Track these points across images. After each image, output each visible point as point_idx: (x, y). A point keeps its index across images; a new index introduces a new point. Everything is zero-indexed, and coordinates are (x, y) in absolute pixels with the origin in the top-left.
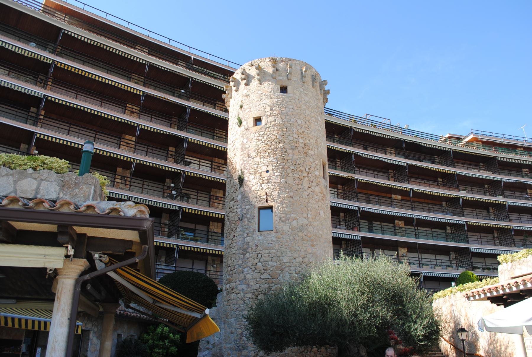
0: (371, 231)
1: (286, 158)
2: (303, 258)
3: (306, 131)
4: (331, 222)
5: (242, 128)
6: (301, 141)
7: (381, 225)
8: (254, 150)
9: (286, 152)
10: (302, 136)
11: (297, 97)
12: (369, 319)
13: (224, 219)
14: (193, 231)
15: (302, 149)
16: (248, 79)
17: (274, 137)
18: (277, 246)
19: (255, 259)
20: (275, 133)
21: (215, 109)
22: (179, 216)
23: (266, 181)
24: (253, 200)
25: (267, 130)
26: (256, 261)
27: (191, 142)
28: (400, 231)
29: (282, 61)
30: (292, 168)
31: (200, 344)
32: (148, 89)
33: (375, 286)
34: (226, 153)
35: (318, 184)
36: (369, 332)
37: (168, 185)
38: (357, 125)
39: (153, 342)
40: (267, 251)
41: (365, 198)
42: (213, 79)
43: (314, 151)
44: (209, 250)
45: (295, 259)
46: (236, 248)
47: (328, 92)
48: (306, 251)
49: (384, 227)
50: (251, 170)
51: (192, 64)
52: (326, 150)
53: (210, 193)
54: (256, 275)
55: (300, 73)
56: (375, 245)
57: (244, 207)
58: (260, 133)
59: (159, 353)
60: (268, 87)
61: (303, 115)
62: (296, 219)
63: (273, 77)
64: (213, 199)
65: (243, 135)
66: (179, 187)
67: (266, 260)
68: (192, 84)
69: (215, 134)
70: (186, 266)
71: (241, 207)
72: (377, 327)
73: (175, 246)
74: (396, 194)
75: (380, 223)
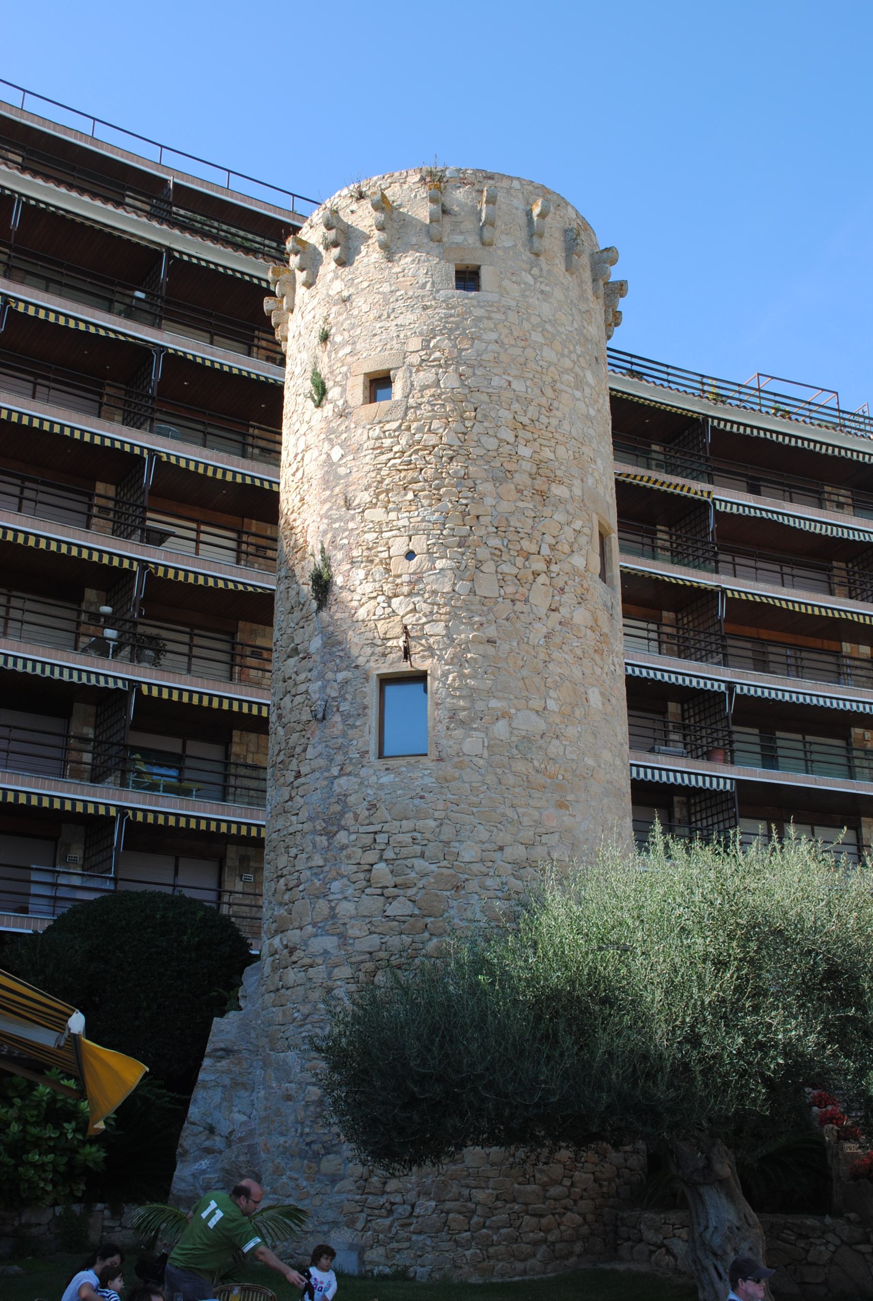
0: (770, 761)
1: (473, 510)
2: (527, 846)
4: (626, 728)
6: (525, 451)
7: (805, 743)
8: (365, 482)
9: (473, 489)
10: (529, 436)
11: (513, 303)
12: (739, 1052)
13: (267, 720)
14: (176, 760)
15: (529, 481)
16: (346, 243)
17: (432, 440)
18: (441, 806)
19: (365, 849)
21: (249, 354)
22: (127, 713)
23: (405, 589)
24: (362, 655)
25: (410, 415)
26: (371, 857)
28: (865, 763)
29: (463, 182)
30: (495, 542)
31: (183, 1134)
32: (19, 287)
33: (764, 940)
34: (273, 498)
35: (581, 600)
36: (741, 1098)
37: (92, 609)
38: (726, 411)
39: (24, 1131)
40: (407, 825)
41: (750, 654)
42: (240, 254)
43: (570, 487)
44: (229, 822)
45: (501, 849)
46: (304, 815)
47: (620, 288)
48: (538, 823)
49: (814, 748)
50: (355, 553)
51: (171, 204)
52: (614, 485)
53: (233, 635)
54: (371, 904)
55: (523, 220)
56: (777, 809)
57: (330, 675)
59: (40, 1167)
60: (413, 266)
61: (531, 365)
62: (505, 715)
63: (433, 236)
64: (243, 656)
65: (330, 435)
66: (128, 616)
67: (405, 852)
68: (169, 269)
69: (250, 440)
70: (153, 876)
71: (321, 676)
72: (767, 1082)
73: (113, 812)
74: (856, 641)
75: (799, 737)
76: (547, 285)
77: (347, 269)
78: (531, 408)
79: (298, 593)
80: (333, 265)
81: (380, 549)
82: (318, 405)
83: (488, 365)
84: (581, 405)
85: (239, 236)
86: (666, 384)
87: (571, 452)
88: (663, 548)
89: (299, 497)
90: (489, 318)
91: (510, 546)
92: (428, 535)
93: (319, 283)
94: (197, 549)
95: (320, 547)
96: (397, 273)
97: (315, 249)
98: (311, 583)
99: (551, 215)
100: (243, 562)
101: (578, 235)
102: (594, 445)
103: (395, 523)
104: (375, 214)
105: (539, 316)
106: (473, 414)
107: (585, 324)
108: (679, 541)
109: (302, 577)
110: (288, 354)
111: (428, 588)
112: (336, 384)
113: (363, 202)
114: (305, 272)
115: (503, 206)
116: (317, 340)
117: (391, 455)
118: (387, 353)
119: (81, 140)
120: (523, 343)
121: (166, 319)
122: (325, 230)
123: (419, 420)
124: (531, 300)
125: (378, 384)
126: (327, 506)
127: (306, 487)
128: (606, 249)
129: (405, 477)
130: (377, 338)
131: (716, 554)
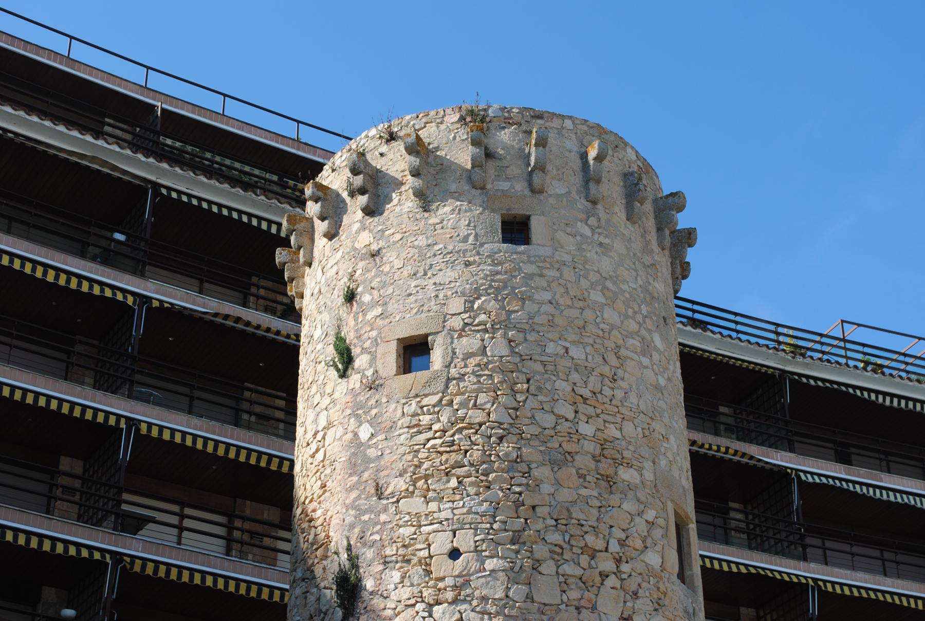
1: (529, 501)
3: (608, 392)
5: (355, 380)
6: (587, 429)
9: (527, 474)
10: (591, 411)
11: (568, 258)
15: (592, 465)
16: (374, 189)
17: (478, 416)
20: (482, 398)
23: (450, 595)
25: (452, 388)
27: (148, 436)
29: (508, 122)
30: (555, 537)
37: (51, 613)
38: (807, 366)
43: (640, 470)
47: (688, 237)
50: (389, 551)
51: (158, 134)
55: (577, 164)
58: (425, 401)
60: (454, 217)
61: (591, 328)
63: (475, 182)
65: (358, 411)
76: (606, 236)
77: (376, 219)
78: (592, 379)
79: (318, 599)
80: (360, 214)
81: (419, 546)
82: (343, 375)
83: (541, 329)
84: (649, 374)
85: (236, 169)
86: (734, 335)
87: (639, 429)
88: (738, 530)
89: (319, 483)
90: (541, 275)
91: (573, 542)
92: (476, 529)
93: (343, 235)
94: (180, 537)
95: (345, 543)
96: (435, 225)
97: (338, 195)
98: (335, 587)
99: (608, 158)
100: (234, 553)
101: (640, 179)
102: (666, 420)
103: (435, 515)
104: (408, 157)
105: (598, 272)
106: (525, 386)
107: (651, 281)
108: (757, 521)
109: (323, 579)
110: (305, 313)
111: (477, 593)
112: (364, 350)
113: (394, 144)
114: (326, 222)
115: (554, 149)
116: (341, 300)
117: (430, 434)
118: (424, 315)
119: (55, 61)
120: (581, 304)
121: (150, 264)
122: (350, 175)
123: (463, 394)
124: (588, 255)
125: (414, 351)
126: (354, 494)
127: (328, 471)
128: (672, 195)
129: (447, 460)
130: (412, 298)
131: (803, 537)
